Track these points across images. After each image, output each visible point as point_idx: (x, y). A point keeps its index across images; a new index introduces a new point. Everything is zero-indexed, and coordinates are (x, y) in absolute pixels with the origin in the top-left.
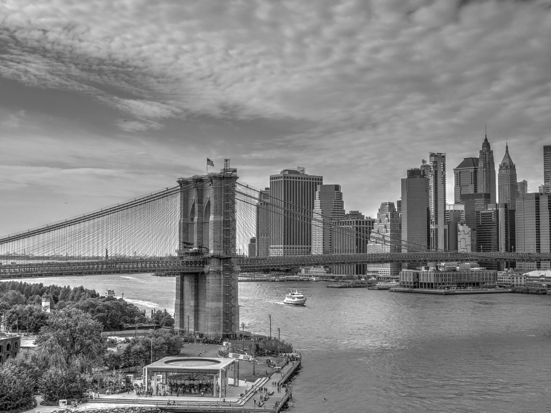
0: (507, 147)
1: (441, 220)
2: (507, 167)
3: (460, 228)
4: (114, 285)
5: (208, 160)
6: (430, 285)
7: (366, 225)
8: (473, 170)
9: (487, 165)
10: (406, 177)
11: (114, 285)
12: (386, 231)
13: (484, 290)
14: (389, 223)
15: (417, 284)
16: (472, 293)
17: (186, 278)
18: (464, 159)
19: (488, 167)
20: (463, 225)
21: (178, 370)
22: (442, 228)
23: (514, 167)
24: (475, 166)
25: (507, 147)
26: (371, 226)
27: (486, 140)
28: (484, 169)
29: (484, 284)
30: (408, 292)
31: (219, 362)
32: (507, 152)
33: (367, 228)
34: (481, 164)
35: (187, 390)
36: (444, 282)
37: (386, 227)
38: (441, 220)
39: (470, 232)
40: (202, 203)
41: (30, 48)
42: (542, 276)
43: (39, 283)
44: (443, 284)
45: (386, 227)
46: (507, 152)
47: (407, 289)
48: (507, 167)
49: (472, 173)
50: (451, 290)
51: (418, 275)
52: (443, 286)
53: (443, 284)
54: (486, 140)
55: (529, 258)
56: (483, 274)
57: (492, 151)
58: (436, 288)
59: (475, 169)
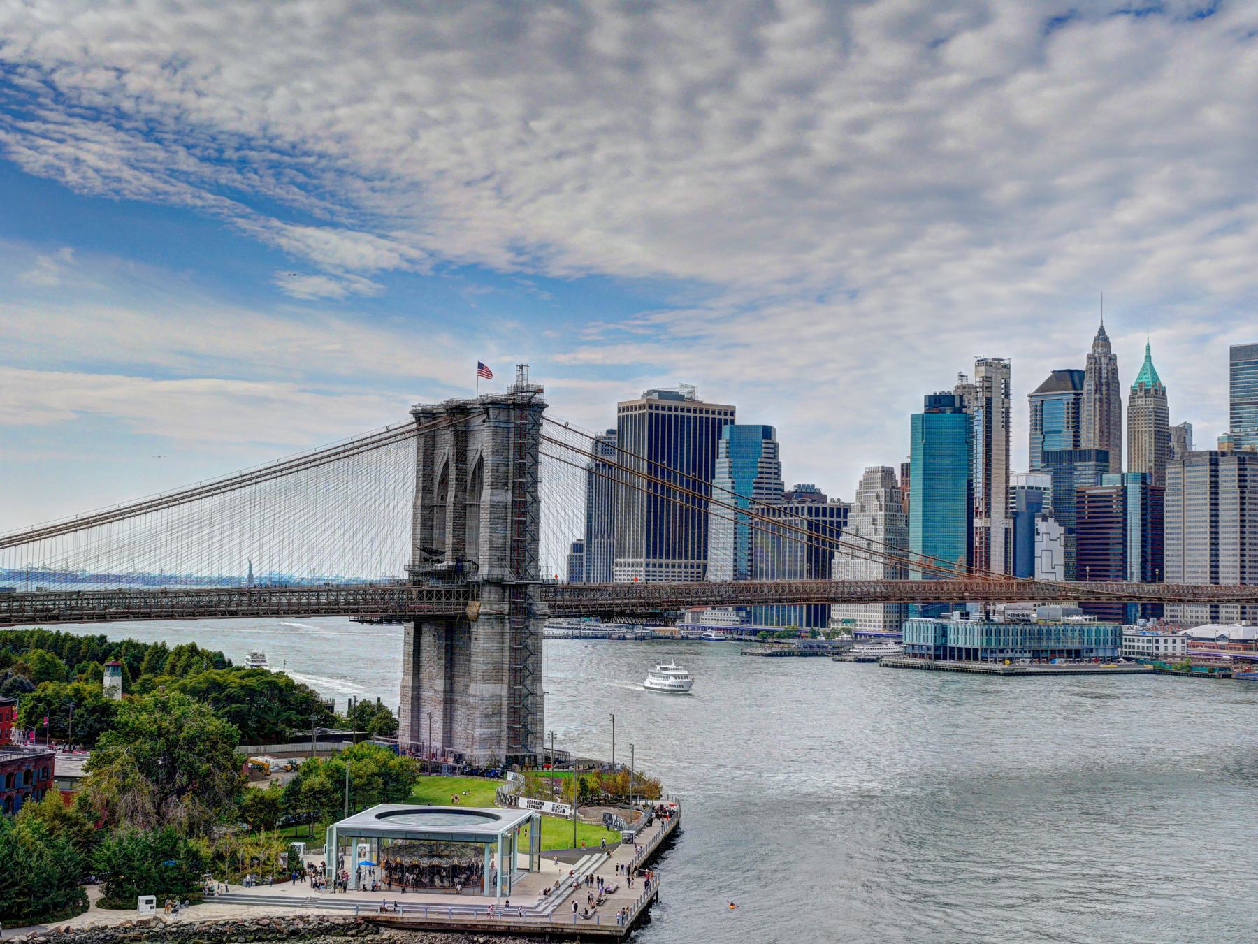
0: (1148, 348)
2: (1147, 391)
3: (1041, 525)
7: (832, 516)
8: (1073, 397)
9: (1104, 388)
12: (876, 530)
14: (883, 513)
18: (1053, 372)
19: (1104, 392)
20: (1047, 521)
23: (1164, 392)
24: (1075, 388)
25: (1148, 348)
26: (842, 519)
27: (1102, 331)
28: (1097, 396)
29: (1092, 652)
31: (496, 818)
32: (1148, 358)
33: (832, 523)
35: (425, 879)
36: (1002, 646)
37: (874, 521)
39: (1062, 537)
41: (86, 108)
42: (1223, 637)
44: (1001, 651)
45: (874, 521)
46: (1148, 358)
48: (1147, 391)
49: (1068, 404)
51: (944, 631)
52: (1001, 655)
53: (1001, 651)
54: (1102, 331)
55: (1192, 596)
56: (1089, 631)
57: (1115, 355)
59: (1075, 394)
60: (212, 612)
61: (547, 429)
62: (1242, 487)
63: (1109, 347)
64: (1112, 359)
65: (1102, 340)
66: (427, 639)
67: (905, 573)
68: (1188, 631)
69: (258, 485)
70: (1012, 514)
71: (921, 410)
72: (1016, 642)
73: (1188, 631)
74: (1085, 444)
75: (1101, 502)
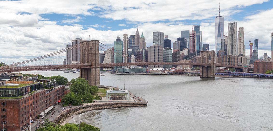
1: (126, 53)
2: (142, 38)
3: (132, 56)
4: (161, 69)
5: (90, 37)
6: (128, 72)
10: (116, 41)
11: (161, 69)
13: (143, 74)
15: (124, 72)
16: (140, 75)
17: (83, 71)
21: (114, 93)
22: (127, 56)
27: (137, 30)
30: (121, 74)
31: (124, 91)
32: (142, 33)
34: (136, 37)
35: (116, 98)
38: (126, 53)
40: (88, 48)
41: (240, 9)
42: (157, 70)
43: (37, 74)
46: (142, 33)
47: (121, 74)
48: (142, 38)
50: (134, 74)
54: (137, 30)
55: (152, 64)
56: (142, 69)
58: (130, 73)
60: (33, 70)
61: (99, 44)
62: (158, 50)
63: (138, 32)
64: (139, 34)
65: (137, 31)
66: (83, 71)
67: (66, 64)
68: (153, 69)
69: (62, 53)
70: (128, 54)
71: (115, 41)
72: (133, 71)
73: (153, 69)
74: (135, 45)
75: (139, 53)
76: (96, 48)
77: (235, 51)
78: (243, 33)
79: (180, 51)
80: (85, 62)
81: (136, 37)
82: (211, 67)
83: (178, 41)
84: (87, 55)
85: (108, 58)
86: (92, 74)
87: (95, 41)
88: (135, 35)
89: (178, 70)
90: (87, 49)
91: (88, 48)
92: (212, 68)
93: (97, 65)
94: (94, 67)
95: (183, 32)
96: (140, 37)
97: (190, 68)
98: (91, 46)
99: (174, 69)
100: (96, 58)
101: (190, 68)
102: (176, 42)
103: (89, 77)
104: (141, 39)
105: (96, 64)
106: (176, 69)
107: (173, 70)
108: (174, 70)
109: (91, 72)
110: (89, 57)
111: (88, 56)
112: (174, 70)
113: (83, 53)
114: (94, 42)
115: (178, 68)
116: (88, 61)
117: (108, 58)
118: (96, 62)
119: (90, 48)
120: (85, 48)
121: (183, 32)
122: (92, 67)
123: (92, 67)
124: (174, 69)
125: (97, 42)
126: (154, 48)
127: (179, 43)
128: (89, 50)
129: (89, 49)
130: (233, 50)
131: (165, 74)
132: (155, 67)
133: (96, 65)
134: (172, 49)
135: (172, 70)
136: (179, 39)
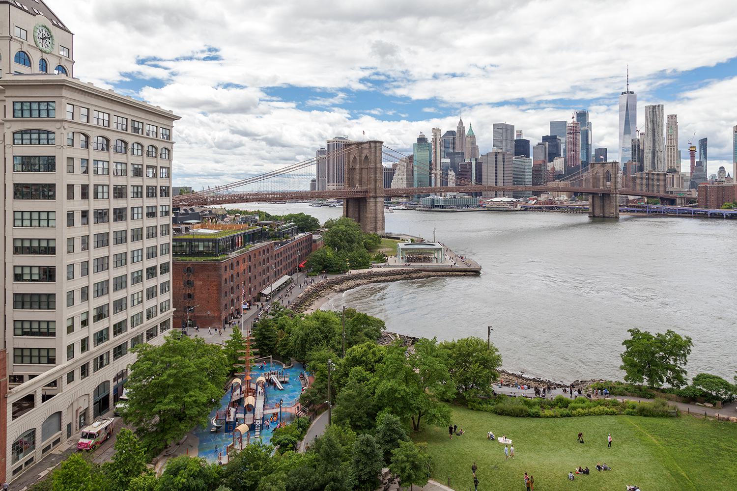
4: (510, 200)
32: (471, 127)
34: (458, 135)
46: (471, 127)
54: (461, 120)
61: (383, 149)
64: (464, 128)
76: (375, 156)
77: (659, 162)
78: (677, 127)
79: (548, 164)
80: (354, 186)
81: (458, 135)
82: (611, 195)
83: (544, 143)
84: (358, 171)
85: (400, 177)
86: (368, 210)
87: (375, 142)
88: (455, 129)
89: (544, 202)
90: (358, 158)
91: (360, 156)
92: (613, 197)
93: (377, 191)
94: (372, 195)
95: (553, 124)
96: (466, 133)
97: (567, 198)
98: (366, 152)
99: (536, 199)
100: (376, 177)
101: (567, 198)
102: (539, 144)
103: (362, 216)
104: (468, 139)
105: (375, 189)
106: (539, 199)
107: (533, 203)
108: (535, 201)
109: (366, 206)
110: (363, 176)
111: (360, 173)
112: (535, 201)
113: (351, 167)
114: (372, 144)
115: (543, 198)
116: (361, 184)
117: (400, 177)
118: (376, 186)
119: (363, 156)
120: (355, 158)
121: (553, 124)
122: (367, 195)
123: (367, 195)
124: (536, 199)
125: (378, 144)
126: (494, 157)
127: (545, 148)
128: (362, 162)
129: (363, 158)
130: (656, 161)
131: (516, 209)
132: (496, 196)
133: (376, 191)
134: (531, 160)
135: (531, 201)
136: (545, 139)
